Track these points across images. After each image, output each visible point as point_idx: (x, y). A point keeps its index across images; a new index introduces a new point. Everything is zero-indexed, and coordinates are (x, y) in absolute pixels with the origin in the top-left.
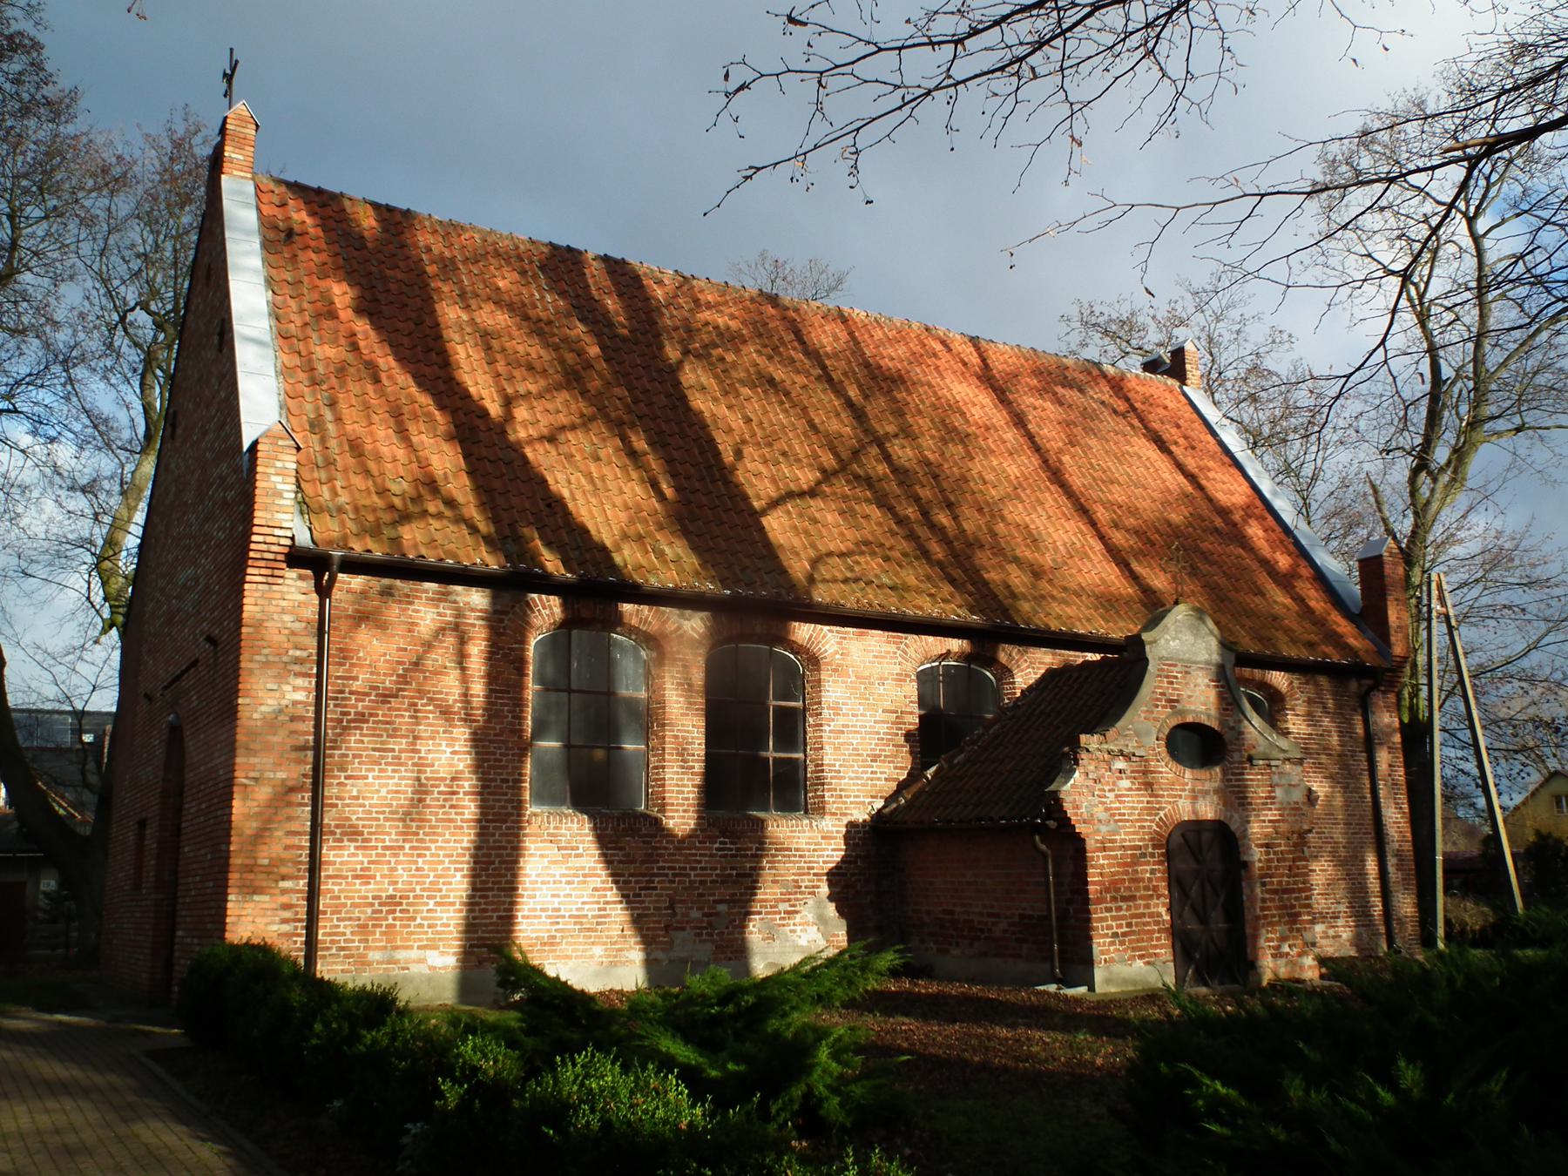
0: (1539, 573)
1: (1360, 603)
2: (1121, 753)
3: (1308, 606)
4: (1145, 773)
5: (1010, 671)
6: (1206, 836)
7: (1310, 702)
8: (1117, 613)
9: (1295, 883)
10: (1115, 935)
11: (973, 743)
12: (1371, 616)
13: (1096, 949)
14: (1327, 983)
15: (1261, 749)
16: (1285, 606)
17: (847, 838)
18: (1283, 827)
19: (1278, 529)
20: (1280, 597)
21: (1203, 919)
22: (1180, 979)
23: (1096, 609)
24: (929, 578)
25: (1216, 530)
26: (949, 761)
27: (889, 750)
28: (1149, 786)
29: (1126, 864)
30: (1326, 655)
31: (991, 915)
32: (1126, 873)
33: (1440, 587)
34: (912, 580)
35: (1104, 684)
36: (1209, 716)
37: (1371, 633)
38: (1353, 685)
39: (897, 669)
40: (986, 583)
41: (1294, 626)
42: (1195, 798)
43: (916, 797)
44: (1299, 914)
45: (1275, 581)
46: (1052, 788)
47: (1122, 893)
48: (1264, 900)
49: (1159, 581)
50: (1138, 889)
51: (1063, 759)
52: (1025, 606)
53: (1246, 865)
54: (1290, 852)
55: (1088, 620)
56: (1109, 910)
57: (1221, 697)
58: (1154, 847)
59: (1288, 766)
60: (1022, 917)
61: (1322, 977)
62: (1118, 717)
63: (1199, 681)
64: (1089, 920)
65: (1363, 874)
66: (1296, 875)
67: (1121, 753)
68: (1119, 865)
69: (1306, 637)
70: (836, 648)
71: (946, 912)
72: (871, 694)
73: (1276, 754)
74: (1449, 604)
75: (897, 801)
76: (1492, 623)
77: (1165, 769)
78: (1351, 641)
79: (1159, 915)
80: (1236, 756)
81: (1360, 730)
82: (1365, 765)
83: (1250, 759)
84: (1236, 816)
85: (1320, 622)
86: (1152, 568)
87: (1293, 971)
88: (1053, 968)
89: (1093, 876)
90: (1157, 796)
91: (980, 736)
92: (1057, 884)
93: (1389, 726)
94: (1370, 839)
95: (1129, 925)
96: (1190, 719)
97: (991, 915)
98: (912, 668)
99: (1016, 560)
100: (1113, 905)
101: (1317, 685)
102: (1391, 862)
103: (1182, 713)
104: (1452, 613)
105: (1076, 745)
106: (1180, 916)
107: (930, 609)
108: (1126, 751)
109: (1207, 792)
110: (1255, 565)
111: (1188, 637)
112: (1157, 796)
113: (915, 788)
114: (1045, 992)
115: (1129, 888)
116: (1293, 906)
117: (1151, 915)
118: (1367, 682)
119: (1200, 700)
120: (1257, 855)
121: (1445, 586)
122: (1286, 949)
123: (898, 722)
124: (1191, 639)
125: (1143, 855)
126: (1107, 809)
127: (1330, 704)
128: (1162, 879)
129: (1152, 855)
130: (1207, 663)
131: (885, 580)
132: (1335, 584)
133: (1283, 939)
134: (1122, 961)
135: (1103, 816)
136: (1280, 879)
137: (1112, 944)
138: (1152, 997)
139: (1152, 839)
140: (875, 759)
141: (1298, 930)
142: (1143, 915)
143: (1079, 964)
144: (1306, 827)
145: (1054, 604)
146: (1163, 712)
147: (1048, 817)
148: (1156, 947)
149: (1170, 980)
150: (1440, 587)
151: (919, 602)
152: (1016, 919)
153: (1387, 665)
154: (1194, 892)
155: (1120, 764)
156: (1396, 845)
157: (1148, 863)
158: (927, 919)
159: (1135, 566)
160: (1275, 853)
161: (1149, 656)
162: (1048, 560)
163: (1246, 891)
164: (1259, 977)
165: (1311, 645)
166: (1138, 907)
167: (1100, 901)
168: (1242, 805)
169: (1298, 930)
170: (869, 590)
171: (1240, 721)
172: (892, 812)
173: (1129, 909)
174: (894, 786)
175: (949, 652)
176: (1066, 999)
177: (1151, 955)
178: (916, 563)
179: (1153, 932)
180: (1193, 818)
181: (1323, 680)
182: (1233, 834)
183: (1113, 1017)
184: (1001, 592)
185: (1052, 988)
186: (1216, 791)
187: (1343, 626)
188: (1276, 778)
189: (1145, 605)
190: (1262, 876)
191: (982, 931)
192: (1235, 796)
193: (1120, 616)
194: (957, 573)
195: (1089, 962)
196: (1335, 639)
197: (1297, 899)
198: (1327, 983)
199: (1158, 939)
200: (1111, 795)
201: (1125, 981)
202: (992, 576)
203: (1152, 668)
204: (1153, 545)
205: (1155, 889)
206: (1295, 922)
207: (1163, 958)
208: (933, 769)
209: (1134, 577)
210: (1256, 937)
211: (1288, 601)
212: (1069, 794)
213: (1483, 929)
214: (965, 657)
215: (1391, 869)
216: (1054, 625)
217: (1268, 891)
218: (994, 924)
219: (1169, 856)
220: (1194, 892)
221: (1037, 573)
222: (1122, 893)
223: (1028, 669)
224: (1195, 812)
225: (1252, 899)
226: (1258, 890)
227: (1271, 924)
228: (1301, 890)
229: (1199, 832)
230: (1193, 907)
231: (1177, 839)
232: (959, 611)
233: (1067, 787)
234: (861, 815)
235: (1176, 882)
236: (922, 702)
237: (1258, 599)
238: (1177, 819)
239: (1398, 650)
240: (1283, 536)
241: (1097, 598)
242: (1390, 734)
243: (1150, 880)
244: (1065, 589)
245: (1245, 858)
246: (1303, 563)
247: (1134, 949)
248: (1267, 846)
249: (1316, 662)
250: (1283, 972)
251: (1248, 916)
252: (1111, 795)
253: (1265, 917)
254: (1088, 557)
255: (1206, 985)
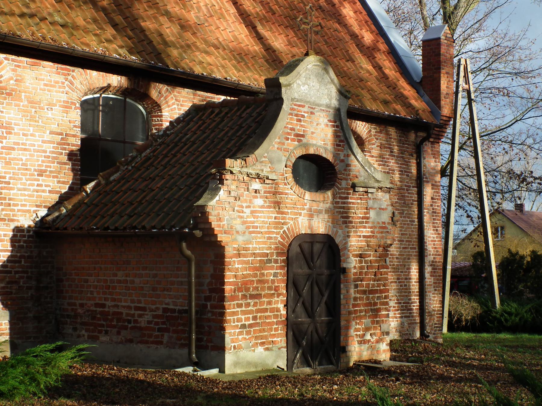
0: (523, 67)
1: (421, 74)
2: (258, 176)
3: (384, 73)
4: (275, 193)
5: (159, 106)
6: (317, 247)
7: (381, 147)
8: (246, 64)
9: (379, 286)
10: (243, 326)
11: (128, 163)
12: (428, 85)
13: (228, 339)
14: (398, 364)
15: (361, 179)
16: (368, 71)
17: (14, 240)
18: (373, 242)
19: (364, 13)
20: (366, 65)
21: (310, 314)
22: (290, 363)
23: (230, 60)
24: (95, 21)
25: (320, 7)
26: (107, 178)
27: (54, 166)
28: (277, 204)
29: (256, 269)
30: (396, 111)
31: (137, 308)
32: (255, 275)
33: (466, 69)
34: (80, 21)
35: (246, 117)
36: (326, 150)
37: (427, 97)
38: (412, 136)
39: (64, 97)
40: (143, 31)
41: (374, 87)
42: (311, 216)
43: (76, 207)
44: (379, 310)
45: (361, 52)
46: (200, 202)
47: (251, 292)
48: (355, 299)
49: (279, 42)
50: (263, 289)
51: (210, 177)
52: (175, 53)
53: (344, 271)
54: (376, 261)
55: (223, 67)
56: (239, 306)
57: (336, 135)
58: (278, 254)
59: (380, 194)
60: (165, 310)
61: (392, 358)
62: (256, 146)
63: (321, 120)
64: (223, 314)
65: (408, 279)
66: (379, 280)
67: (258, 176)
68: (250, 269)
69: (383, 96)
70: (11, 74)
71: (97, 305)
72: (40, 117)
73: (372, 183)
74: (471, 82)
75: (59, 210)
76: (488, 101)
77: (292, 192)
78: (413, 102)
79: (278, 310)
80: (344, 183)
81: (414, 171)
82: (415, 197)
83: (354, 186)
84: (340, 231)
85: (393, 87)
86: (271, 30)
87: (372, 354)
88: (190, 354)
89: (229, 277)
90: (283, 213)
91: (134, 158)
92: (199, 284)
93: (433, 169)
94: (415, 252)
95: (255, 318)
96: (311, 151)
97: (137, 308)
98: (78, 96)
99: (167, 14)
100: (243, 302)
101: (387, 134)
102: (428, 269)
103: (306, 146)
104: (472, 89)
105: (221, 167)
106: (294, 311)
107: (93, 45)
108: (262, 174)
109: (319, 212)
110: (347, 38)
111: (314, 83)
112: (283, 213)
113: (75, 200)
114: (184, 374)
115: (256, 288)
116: (375, 304)
117: (272, 310)
118: (422, 134)
119: (321, 138)
120: (352, 263)
121: (469, 70)
122: (368, 337)
123: (63, 143)
124: (317, 86)
125: (269, 261)
126: (244, 223)
127: (396, 149)
128: (282, 281)
129: (276, 261)
130: (328, 106)
131: (57, 18)
132: (404, 59)
133: (367, 329)
134: (248, 347)
135: (240, 227)
136: (366, 283)
137: (241, 333)
138: (272, 377)
139: (277, 248)
140: (41, 173)
141: (378, 322)
142: (266, 310)
143: (211, 348)
144: (389, 242)
145: (197, 53)
146: (291, 144)
147: (195, 227)
148: (274, 336)
149: (283, 364)
150: (466, 69)
151: (87, 40)
152: (160, 312)
153: (436, 122)
154: (305, 291)
155: (256, 185)
156: (431, 258)
157: (272, 268)
158: (80, 311)
159: (260, 28)
160: (366, 262)
161: (284, 96)
162: (192, 16)
163: (343, 291)
164: (348, 359)
165: (386, 103)
166: (262, 304)
167: (233, 298)
168: (345, 222)
169: (378, 322)
170: (42, 25)
171: (348, 156)
172: (54, 220)
173: (255, 305)
174: (55, 198)
175: (109, 86)
176: (203, 380)
177: (269, 343)
178: (84, 7)
179: (271, 324)
180: (309, 232)
181: (392, 131)
182: (337, 246)
183: (245, 397)
184: (156, 39)
185: (189, 370)
186: (327, 211)
187: (408, 91)
188: (371, 202)
189: (267, 61)
190: (355, 280)
191: (129, 322)
192: (341, 215)
193: (248, 67)
194: (119, 19)
195: (221, 348)
196: (402, 99)
197: (378, 298)
198: (398, 364)
199: (276, 329)
200: (248, 211)
201: (249, 364)
202: (148, 25)
203: (286, 107)
204: (274, 14)
205: (277, 289)
206: (376, 316)
207: (279, 345)
208: (92, 184)
209: (260, 38)
210: (348, 328)
211: (370, 68)
212: (213, 207)
213: (473, 318)
214: (124, 92)
215: (427, 275)
216: (198, 70)
217: (358, 292)
218: (140, 316)
219: (288, 263)
220: (305, 291)
221: (184, 26)
222: (251, 292)
223: (174, 105)
224: (310, 227)
225: (347, 298)
226: (352, 291)
227: (360, 317)
228: (381, 291)
229: (312, 243)
230: (303, 303)
231: (296, 249)
232: (121, 51)
233: (213, 203)
234: (26, 221)
235: (293, 284)
236: (83, 128)
237: (349, 64)
238: (297, 232)
239: (446, 111)
240: (367, 18)
241: (231, 51)
242: (434, 175)
243: (273, 281)
244: (206, 41)
245: (344, 265)
246: (381, 40)
247: (256, 338)
248: (361, 256)
249: (389, 116)
250: (366, 355)
251: (343, 311)
252: (248, 211)
253: (356, 312)
254: (224, 18)
255: (309, 366)
